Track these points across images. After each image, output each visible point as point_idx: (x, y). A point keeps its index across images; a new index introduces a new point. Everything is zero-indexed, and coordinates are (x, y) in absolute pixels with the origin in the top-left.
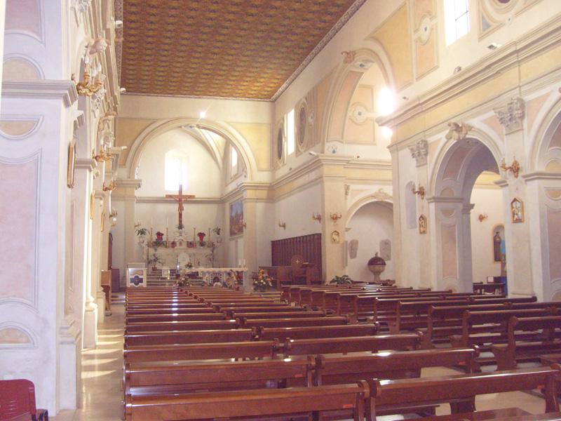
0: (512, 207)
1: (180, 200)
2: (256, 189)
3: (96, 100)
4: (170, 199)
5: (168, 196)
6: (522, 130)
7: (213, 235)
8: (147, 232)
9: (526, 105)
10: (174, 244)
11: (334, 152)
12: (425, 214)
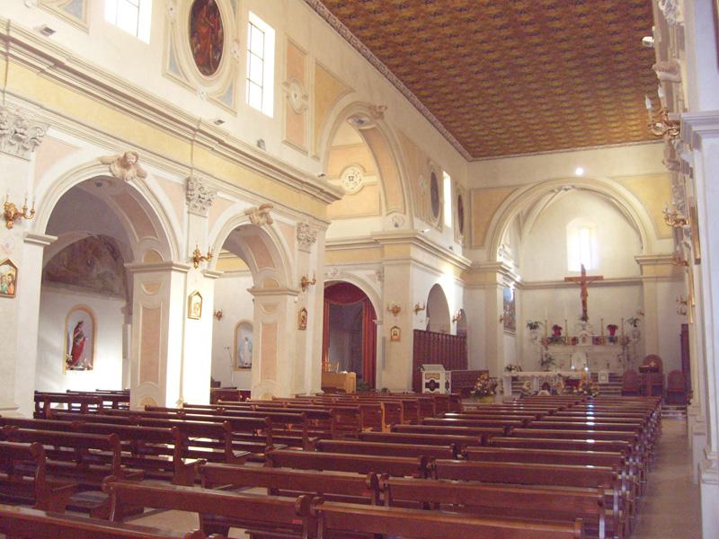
1: (583, 282)
2: (655, 265)
3: (192, 203)
4: (570, 282)
7: (628, 329)
8: (541, 326)
10: (575, 340)
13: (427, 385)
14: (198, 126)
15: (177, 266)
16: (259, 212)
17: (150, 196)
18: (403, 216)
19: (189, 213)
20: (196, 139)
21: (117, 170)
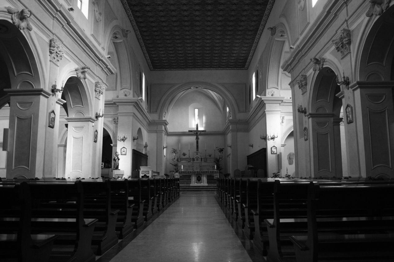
0: (346, 112)
3: (53, 55)
5: (191, 131)
6: (350, 53)
16: (82, 71)
18: (129, 90)
21: (17, 21)
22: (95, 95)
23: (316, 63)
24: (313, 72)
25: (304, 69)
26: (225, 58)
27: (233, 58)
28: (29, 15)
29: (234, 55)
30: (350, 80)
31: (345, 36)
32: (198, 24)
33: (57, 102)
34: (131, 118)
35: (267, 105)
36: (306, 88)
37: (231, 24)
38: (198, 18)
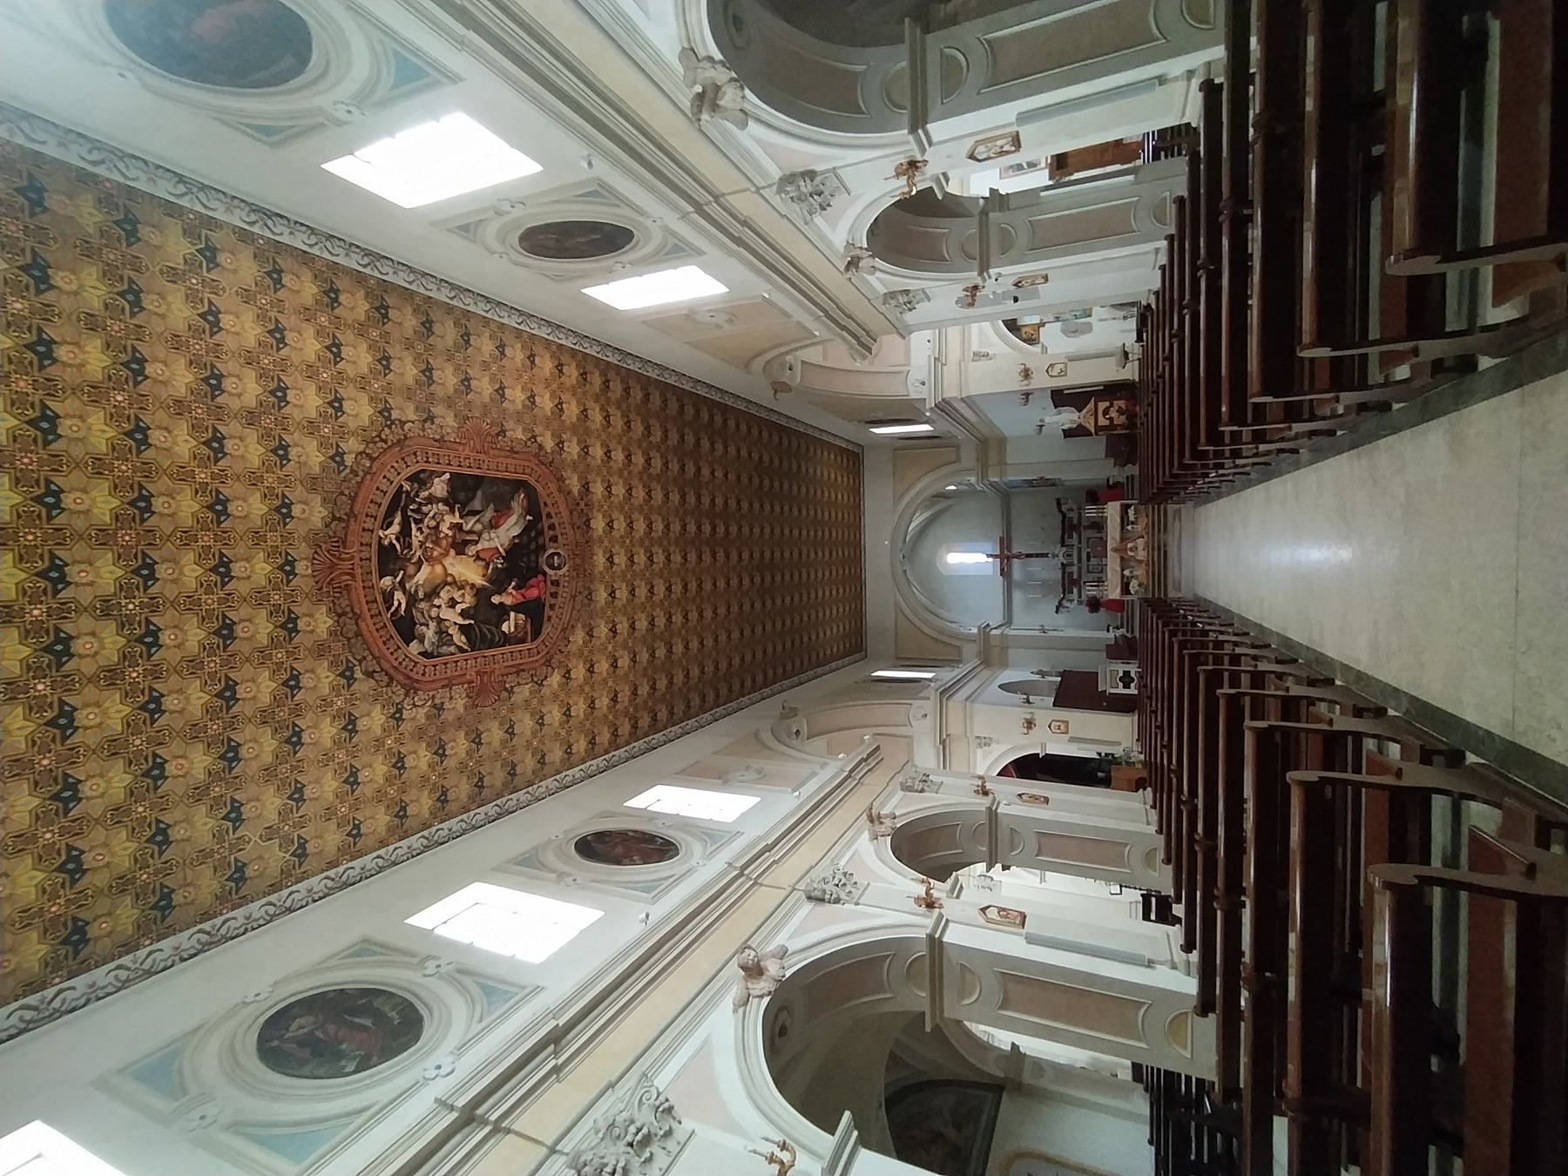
0: (989, 158)
3: (843, 896)
4: (1005, 572)
6: (834, 168)
9: (788, 173)
11: (923, 384)
12: (1014, 279)
13: (1126, 686)
14: (735, 868)
15: (935, 929)
16: (876, 822)
17: (820, 948)
19: (857, 904)
20: (754, 877)
21: (763, 986)
22: (931, 792)
23: (857, 267)
24: (878, 274)
25: (869, 300)
26: (840, 496)
27: (839, 478)
28: (753, 953)
29: (833, 476)
30: (903, 161)
31: (793, 188)
32: (767, 555)
33: (958, 897)
34: (977, 706)
35: (947, 395)
36: (914, 291)
37: (767, 483)
38: (757, 555)
